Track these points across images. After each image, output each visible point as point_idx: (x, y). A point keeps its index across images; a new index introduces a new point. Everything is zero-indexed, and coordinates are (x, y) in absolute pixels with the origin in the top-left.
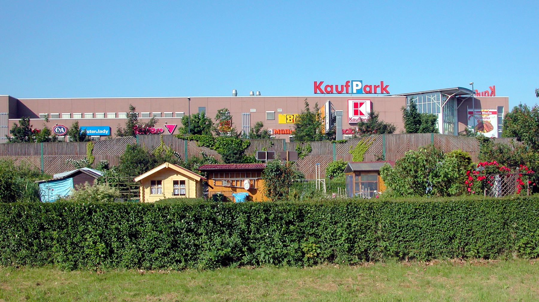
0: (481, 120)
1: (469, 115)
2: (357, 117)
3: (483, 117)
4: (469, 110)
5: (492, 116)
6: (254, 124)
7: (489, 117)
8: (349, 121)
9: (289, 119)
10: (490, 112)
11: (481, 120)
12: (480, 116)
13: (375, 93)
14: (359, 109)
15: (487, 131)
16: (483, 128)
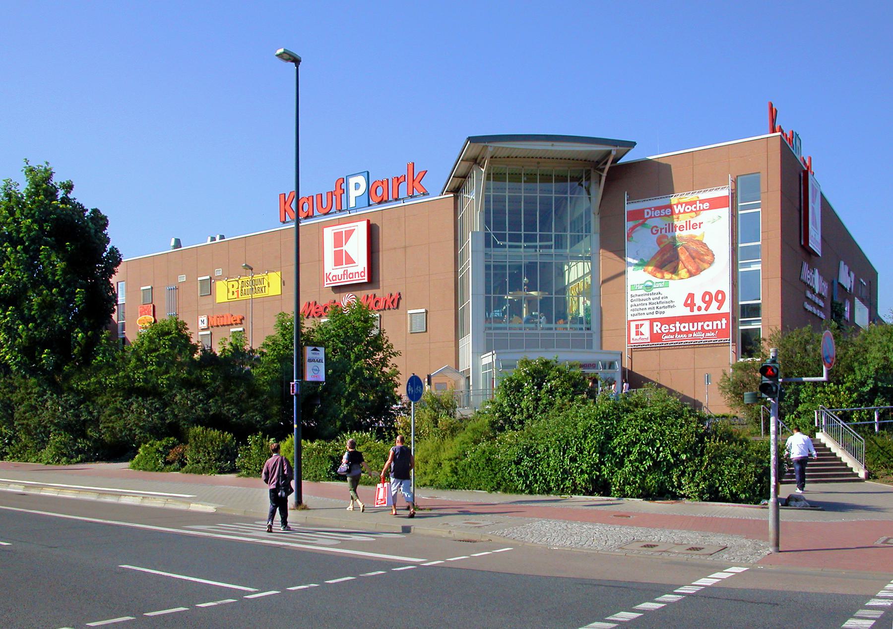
0: (669, 235)
1: (628, 225)
2: (638, 337)
3: (676, 222)
4: (629, 207)
5: (707, 216)
6: (275, 321)
7: (697, 220)
8: (326, 283)
9: (231, 290)
10: (702, 202)
11: (669, 235)
12: (667, 220)
13: (396, 200)
14: (344, 248)
15: (689, 271)
16: (673, 264)
